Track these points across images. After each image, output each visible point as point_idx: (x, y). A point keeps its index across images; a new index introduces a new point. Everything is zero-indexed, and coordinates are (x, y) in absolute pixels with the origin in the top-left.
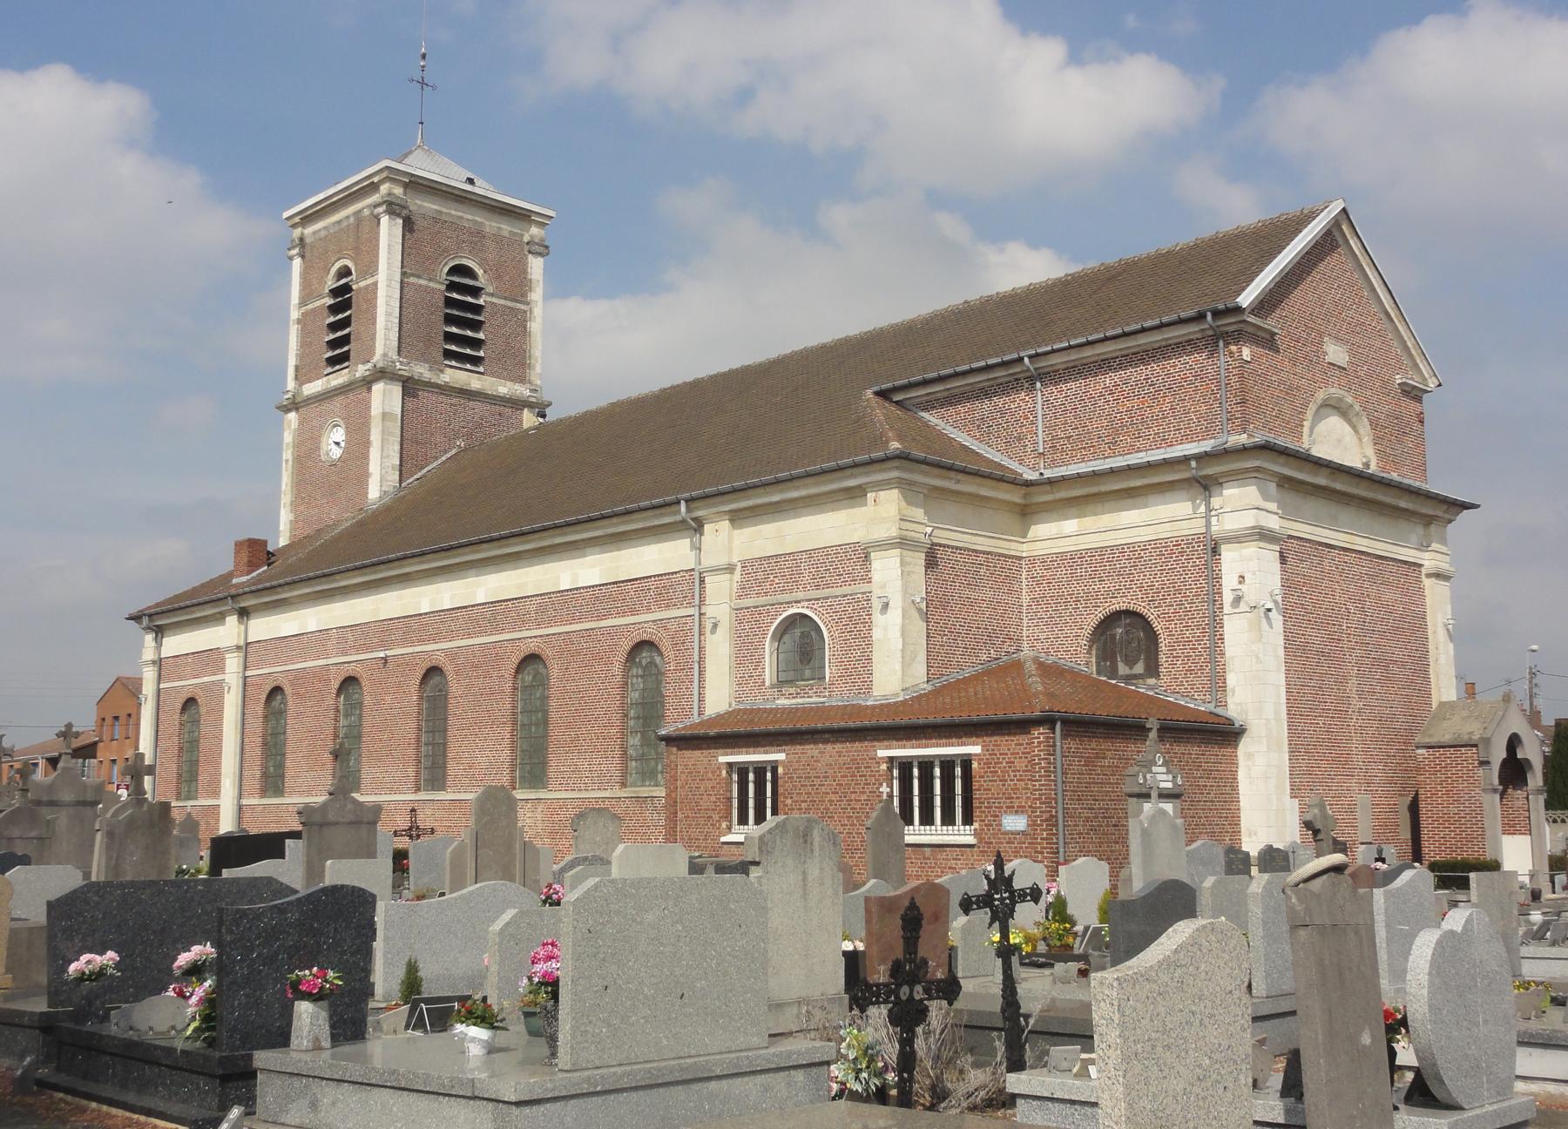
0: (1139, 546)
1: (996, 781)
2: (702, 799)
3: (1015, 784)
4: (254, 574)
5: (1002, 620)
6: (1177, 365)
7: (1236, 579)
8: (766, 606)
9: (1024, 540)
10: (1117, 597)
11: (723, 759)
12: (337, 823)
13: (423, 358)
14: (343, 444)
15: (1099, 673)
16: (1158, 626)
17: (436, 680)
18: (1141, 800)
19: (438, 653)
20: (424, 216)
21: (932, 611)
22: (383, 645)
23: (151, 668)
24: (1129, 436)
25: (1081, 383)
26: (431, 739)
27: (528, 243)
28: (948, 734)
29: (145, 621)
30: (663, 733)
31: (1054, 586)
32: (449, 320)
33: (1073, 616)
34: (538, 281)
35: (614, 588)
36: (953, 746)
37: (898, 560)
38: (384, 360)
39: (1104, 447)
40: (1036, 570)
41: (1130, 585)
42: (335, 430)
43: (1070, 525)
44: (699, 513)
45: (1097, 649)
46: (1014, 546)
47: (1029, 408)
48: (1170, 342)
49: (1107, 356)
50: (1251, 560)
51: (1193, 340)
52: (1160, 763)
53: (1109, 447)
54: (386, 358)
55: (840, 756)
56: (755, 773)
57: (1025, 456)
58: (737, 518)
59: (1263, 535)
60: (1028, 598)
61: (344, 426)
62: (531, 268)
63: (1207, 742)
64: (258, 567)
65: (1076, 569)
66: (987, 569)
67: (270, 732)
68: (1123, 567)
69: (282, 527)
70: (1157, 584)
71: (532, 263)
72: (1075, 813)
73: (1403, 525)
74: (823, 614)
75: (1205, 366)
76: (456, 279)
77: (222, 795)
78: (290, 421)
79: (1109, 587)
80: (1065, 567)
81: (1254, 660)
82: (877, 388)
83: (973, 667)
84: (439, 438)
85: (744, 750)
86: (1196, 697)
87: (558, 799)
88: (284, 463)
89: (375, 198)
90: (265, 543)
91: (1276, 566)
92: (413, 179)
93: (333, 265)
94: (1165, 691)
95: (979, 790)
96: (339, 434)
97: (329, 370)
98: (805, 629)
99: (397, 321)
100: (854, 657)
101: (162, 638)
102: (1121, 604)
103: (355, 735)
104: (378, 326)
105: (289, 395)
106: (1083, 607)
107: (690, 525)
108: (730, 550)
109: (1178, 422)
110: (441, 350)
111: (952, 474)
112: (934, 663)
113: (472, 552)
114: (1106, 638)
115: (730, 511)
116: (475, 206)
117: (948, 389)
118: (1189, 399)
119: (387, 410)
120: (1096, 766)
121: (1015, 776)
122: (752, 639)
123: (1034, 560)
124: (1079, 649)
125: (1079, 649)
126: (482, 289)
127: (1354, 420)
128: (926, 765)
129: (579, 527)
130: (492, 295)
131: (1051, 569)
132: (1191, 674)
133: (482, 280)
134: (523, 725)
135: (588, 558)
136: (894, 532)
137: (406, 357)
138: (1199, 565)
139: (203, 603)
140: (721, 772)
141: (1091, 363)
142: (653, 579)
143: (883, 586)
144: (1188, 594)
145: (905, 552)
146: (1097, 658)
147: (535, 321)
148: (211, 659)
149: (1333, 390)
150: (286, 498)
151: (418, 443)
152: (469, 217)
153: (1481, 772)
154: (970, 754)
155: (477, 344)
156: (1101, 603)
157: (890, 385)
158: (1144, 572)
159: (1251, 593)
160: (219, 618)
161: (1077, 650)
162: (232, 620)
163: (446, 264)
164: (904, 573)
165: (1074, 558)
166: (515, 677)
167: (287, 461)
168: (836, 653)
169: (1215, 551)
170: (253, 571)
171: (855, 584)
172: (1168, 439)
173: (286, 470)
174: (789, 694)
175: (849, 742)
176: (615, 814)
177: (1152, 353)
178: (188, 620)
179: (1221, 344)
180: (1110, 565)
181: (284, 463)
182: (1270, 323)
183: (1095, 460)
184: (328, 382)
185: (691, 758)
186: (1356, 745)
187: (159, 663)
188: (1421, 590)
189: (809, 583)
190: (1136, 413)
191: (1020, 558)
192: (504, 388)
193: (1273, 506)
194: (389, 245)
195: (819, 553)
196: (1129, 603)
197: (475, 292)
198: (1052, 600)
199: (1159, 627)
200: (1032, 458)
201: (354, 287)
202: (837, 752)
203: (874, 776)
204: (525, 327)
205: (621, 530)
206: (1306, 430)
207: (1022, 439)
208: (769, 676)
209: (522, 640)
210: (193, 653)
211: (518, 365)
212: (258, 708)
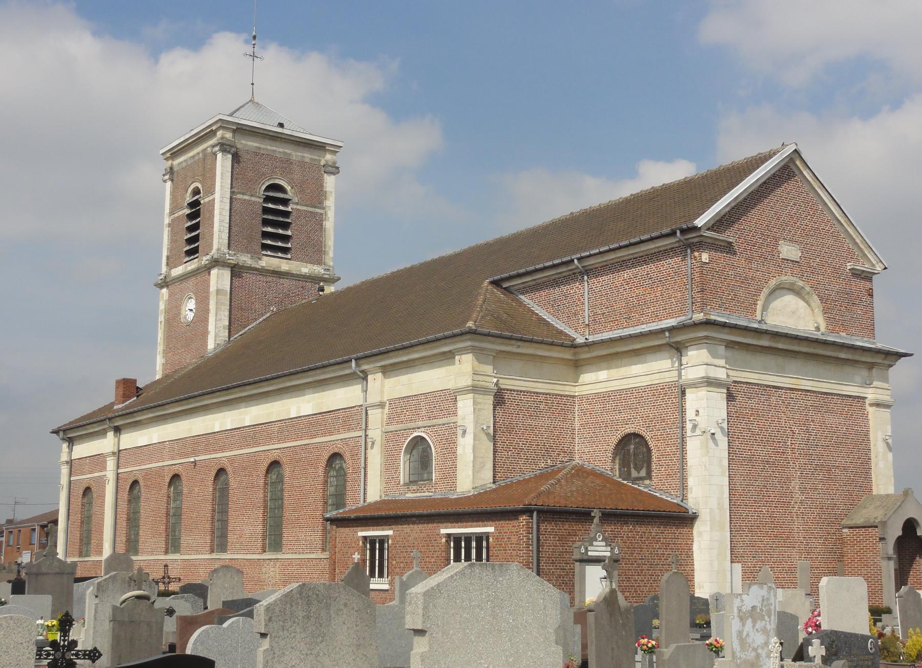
0: (642, 389)
1: (501, 550)
2: (349, 560)
3: (511, 553)
4: (127, 403)
5: (558, 439)
6: (665, 265)
7: (694, 413)
8: (401, 430)
9: (577, 384)
10: (628, 424)
11: (361, 534)
12: (46, 574)
14: (194, 310)
15: (620, 477)
16: (651, 444)
17: (337, 463)
18: (583, 564)
19: (224, 459)
20: (247, 152)
21: (500, 434)
22: (195, 453)
23: (66, 467)
24: (637, 313)
25: (610, 277)
26: (220, 517)
27: (324, 166)
28: (498, 518)
29: (61, 434)
30: (328, 516)
31: (593, 416)
32: (266, 222)
33: (604, 436)
34: (331, 192)
35: (319, 417)
36: (480, 527)
37: (472, 400)
38: (218, 253)
39: (623, 321)
40: (583, 405)
41: (636, 416)
42: (190, 300)
43: (603, 375)
44: (365, 367)
45: (620, 460)
46: (568, 388)
47: (581, 293)
48: (661, 249)
49: (624, 259)
50: (703, 400)
51: (674, 248)
52: (600, 539)
53: (626, 321)
54: (219, 252)
55: (421, 533)
56: (370, 544)
57: (578, 326)
58: (386, 371)
59: (710, 382)
60: (579, 424)
61: (194, 298)
62: (326, 183)
63: (666, 525)
64: (130, 398)
65: (606, 404)
66: (545, 405)
67: (132, 511)
68: (633, 404)
69: (158, 368)
70: (651, 415)
71: (327, 179)
72: (550, 572)
73: (848, 369)
74: (432, 437)
75: (681, 266)
76: (271, 194)
77: (103, 553)
78: (163, 294)
79: (624, 417)
80: (600, 403)
81: (703, 468)
82: (491, 279)
83: (533, 472)
84: (257, 306)
85: (372, 528)
86: (672, 493)
87: (287, 559)
88: (159, 323)
89: (213, 141)
90: (135, 381)
92: (239, 127)
93: (190, 186)
94: (655, 489)
95: (492, 556)
96: (192, 304)
97: (187, 259)
98: (424, 447)
99: (228, 225)
100: (449, 466)
101: (73, 446)
102: (631, 429)
103: (178, 514)
104: (215, 229)
105: (162, 277)
106: (609, 431)
107: (358, 375)
108: (382, 392)
109: (665, 304)
110: (260, 244)
111: (513, 342)
112: (501, 470)
113: (241, 391)
114: (625, 452)
115: (382, 366)
116: (285, 142)
117: (535, 280)
118: (672, 288)
119: (220, 287)
120: (569, 541)
121: (511, 547)
122: (394, 453)
123: (582, 398)
124: (607, 459)
125: (607, 459)
126: (290, 200)
127: (806, 297)
128: (468, 538)
129: (299, 376)
130: (297, 204)
131: (592, 404)
132: (669, 477)
133: (290, 194)
134: (271, 508)
135: (306, 396)
136: (470, 383)
138: (675, 403)
139: (129, 414)
140: (359, 542)
141: (616, 263)
142: (341, 411)
143: (464, 419)
144: (669, 422)
145: (477, 396)
146: (620, 464)
147: (328, 221)
148: (98, 461)
149: (784, 278)
150: (160, 348)
151: (242, 309)
152: (281, 150)
153: (880, 545)
154: (488, 533)
155: (286, 238)
156: (620, 428)
157: (498, 277)
158: (644, 407)
159: (702, 421)
160: (102, 433)
161: (605, 460)
162: (111, 434)
163: (263, 183)
164: (477, 410)
165: (605, 397)
166: (266, 476)
167: (161, 322)
168: (439, 463)
169: (683, 393)
170: (126, 401)
171: (449, 417)
172: (659, 316)
173: (161, 329)
174: (413, 490)
175: (427, 523)
176: (238, 569)
177: (651, 257)
178: (86, 434)
179: (689, 251)
180: (625, 402)
181: (159, 323)
182: (729, 236)
183: (618, 329)
184: (186, 267)
185: (344, 532)
186: (797, 525)
187: (70, 463)
188: (865, 416)
189: (425, 416)
190: (641, 298)
191: (574, 397)
192: (306, 269)
193: (722, 362)
194: (222, 173)
195: (431, 395)
196: (636, 428)
197: (285, 202)
198: (592, 425)
199: (652, 445)
200: (582, 328)
201: (202, 202)
202: (420, 530)
203: (439, 546)
204: (322, 225)
205: (322, 378)
206: (759, 307)
207: (577, 315)
208: (403, 477)
209: (270, 451)
210: (89, 457)
211: (316, 253)
212: (124, 495)
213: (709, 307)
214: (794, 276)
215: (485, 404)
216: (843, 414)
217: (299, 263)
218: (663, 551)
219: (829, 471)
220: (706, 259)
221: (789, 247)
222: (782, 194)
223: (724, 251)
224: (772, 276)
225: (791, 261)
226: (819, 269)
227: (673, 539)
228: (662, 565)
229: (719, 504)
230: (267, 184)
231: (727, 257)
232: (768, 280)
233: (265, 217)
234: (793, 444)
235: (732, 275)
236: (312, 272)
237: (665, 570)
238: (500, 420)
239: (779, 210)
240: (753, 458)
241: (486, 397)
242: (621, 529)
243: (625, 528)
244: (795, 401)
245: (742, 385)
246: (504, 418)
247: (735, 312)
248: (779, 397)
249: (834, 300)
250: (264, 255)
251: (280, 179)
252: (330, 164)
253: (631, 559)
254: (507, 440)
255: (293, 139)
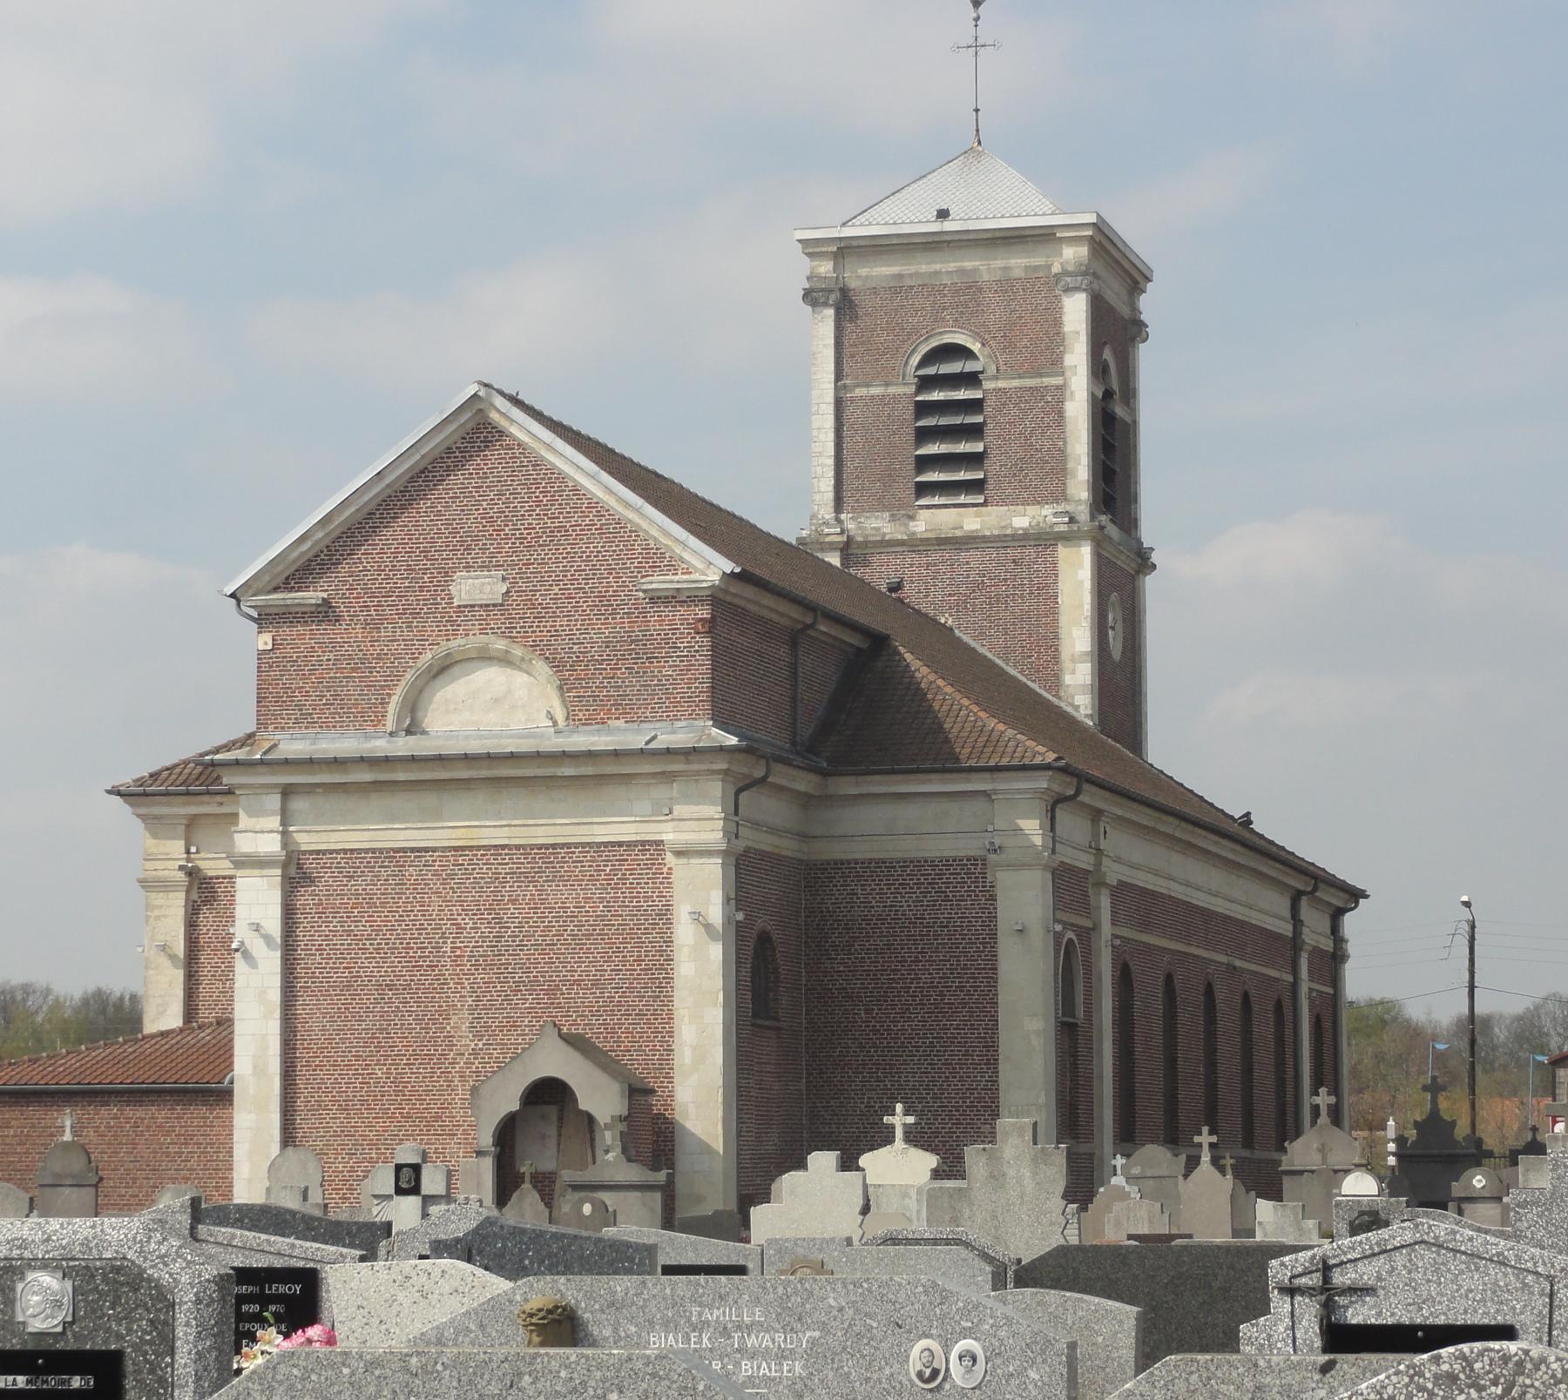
13: (880, 505)
20: (875, 291)
34: (1078, 333)
91: (275, 897)
116: (960, 247)
126: (982, 372)
127: (524, 666)
130: (996, 378)
137: (854, 510)
152: (952, 266)
163: (914, 351)
164: (151, 920)
192: (1022, 519)
197: (972, 379)
213: (271, 728)
214: (487, 634)
215: (169, 906)
216: (598, 880)
217: (1006, 508)
218: (180, 1148)
219: (552, 991)
220: (266, 644)
221: (476, 581)
222: (466, 481)
223: (313, 621)
224: (430, 645)
225: (481, 606)
226: (557, 608)
227: (202, 1126)
228: (176, 1170)
229: (255, 1067)
230: (924, 349)
231: (318, 630)
232: (420, 653)
233: (920, 424)
234: (459, 948)
235: (329, 660)
236: (1038, 523)
237: (183, 1178)
238: (208, 930)
239: (459, 515)
240: (357, 981)
241: (171, 895)
242: (95, 1114)
243: (103, 1111)
244: (466, 869)
245: (334, 855)
246: (218, 926)
247: (334, 727)
248: (424, 866)
249: (597, 660)
250: (922, 507)
251: (955, 332)
252: (1071, 268)
253: (114, 1162)
254: (223, 963)
255: (972, 237)
